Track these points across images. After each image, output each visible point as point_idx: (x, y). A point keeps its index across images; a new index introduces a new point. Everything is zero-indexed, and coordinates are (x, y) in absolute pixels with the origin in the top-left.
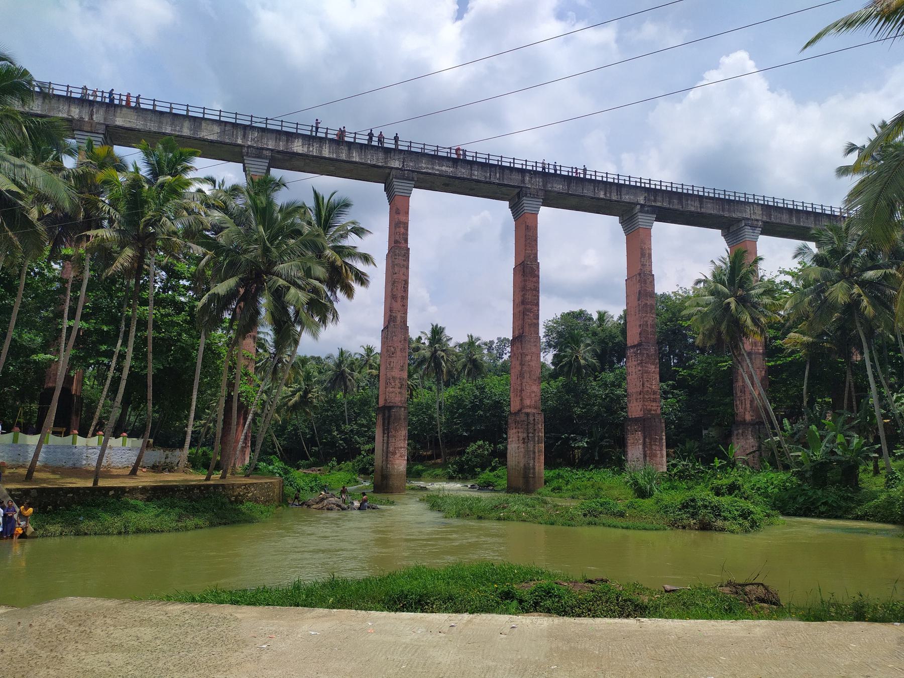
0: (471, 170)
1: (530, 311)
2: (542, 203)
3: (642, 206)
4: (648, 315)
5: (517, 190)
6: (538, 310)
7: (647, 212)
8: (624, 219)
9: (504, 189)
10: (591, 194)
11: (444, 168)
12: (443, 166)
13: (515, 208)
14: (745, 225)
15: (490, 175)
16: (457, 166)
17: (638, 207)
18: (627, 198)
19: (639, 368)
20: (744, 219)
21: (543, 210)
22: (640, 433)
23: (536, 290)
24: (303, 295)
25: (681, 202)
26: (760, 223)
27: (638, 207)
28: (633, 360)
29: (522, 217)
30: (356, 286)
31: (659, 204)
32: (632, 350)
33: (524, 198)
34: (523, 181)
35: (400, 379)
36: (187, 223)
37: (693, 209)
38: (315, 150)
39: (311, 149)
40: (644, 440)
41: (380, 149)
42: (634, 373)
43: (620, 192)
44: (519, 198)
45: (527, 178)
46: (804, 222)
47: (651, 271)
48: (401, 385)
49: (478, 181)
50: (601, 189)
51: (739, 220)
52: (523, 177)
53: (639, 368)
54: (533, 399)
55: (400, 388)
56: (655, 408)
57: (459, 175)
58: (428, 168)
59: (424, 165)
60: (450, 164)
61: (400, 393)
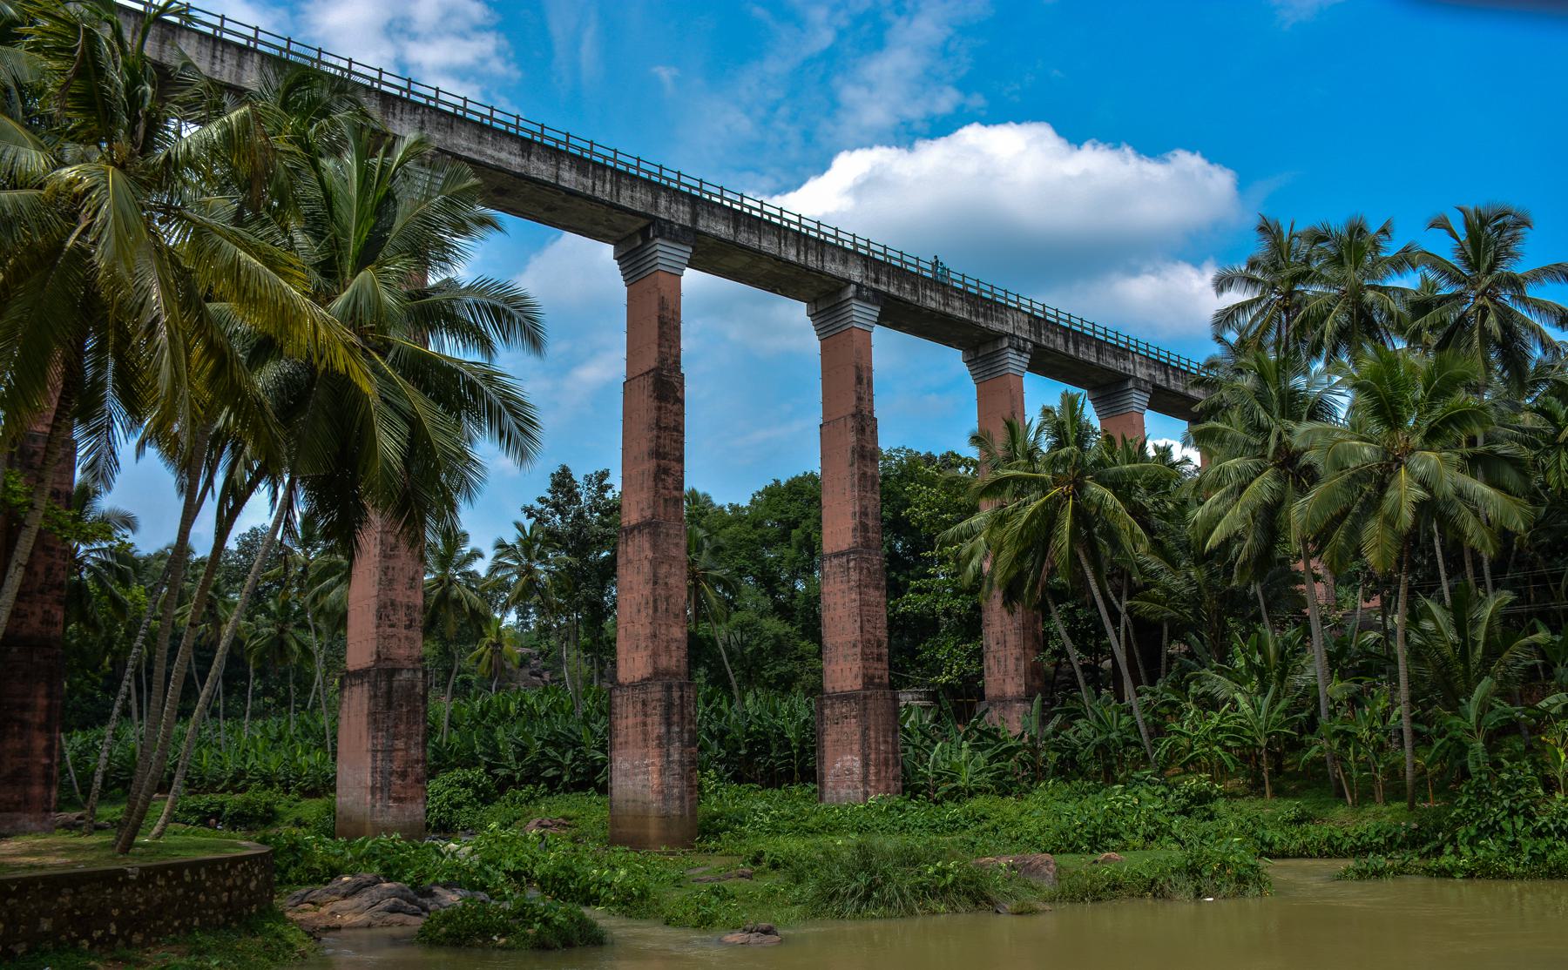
0: (558, 169)
1: (666, 471)
2: (690, 260)
3: (859, 286)
4: (869, 495)
5: (642, 223)
6: (682, 472)
7: (867, 300)
8: (820, 308)
9: (617, 218)
10: (774, 250)
11: (503, 155)
12: (502, 149)
13: (632, 261)
14: (1009, 346)
15: (594, 184)
16: (529, 155)
17: (853, 288)
18: (833, 268)
19: (853, 596)
20: (1007, 334)
21: (688, 272)
22: (853, 721)
23: (678, 431)
24: (181, 955)
25: (915, 290)
26: (1029, 346)
27: (853, 288)
28: (838, 580)
29: (653, 276)
30: (510, 360)
31: (883, 288)
32: (835, 562)
33: (658, 240)
34: (655, 205)
35: (408, 607)
36: (795, 849)
37: (933, 305)
38: (226, 72)
39: (217, 68)
40: (864, 735)
41: (373, 94)
42: (839, 606)
43: (823, 257)
44: (646, 239)
45: (663, 203)
46: (1084, 353)
47: (871, 412)
48: (411, 621)
49: (571, 193)
50: (791, 245)
51: (999, 336)
52: (656, 198)
53: (853, 596)
54: (674, 654)
55: (408, 627)
56: (880, 673)
57: (533, 173)
58: (470, 150)
59: (464, 143)
60: (516, 147)
61: (407, 638)
